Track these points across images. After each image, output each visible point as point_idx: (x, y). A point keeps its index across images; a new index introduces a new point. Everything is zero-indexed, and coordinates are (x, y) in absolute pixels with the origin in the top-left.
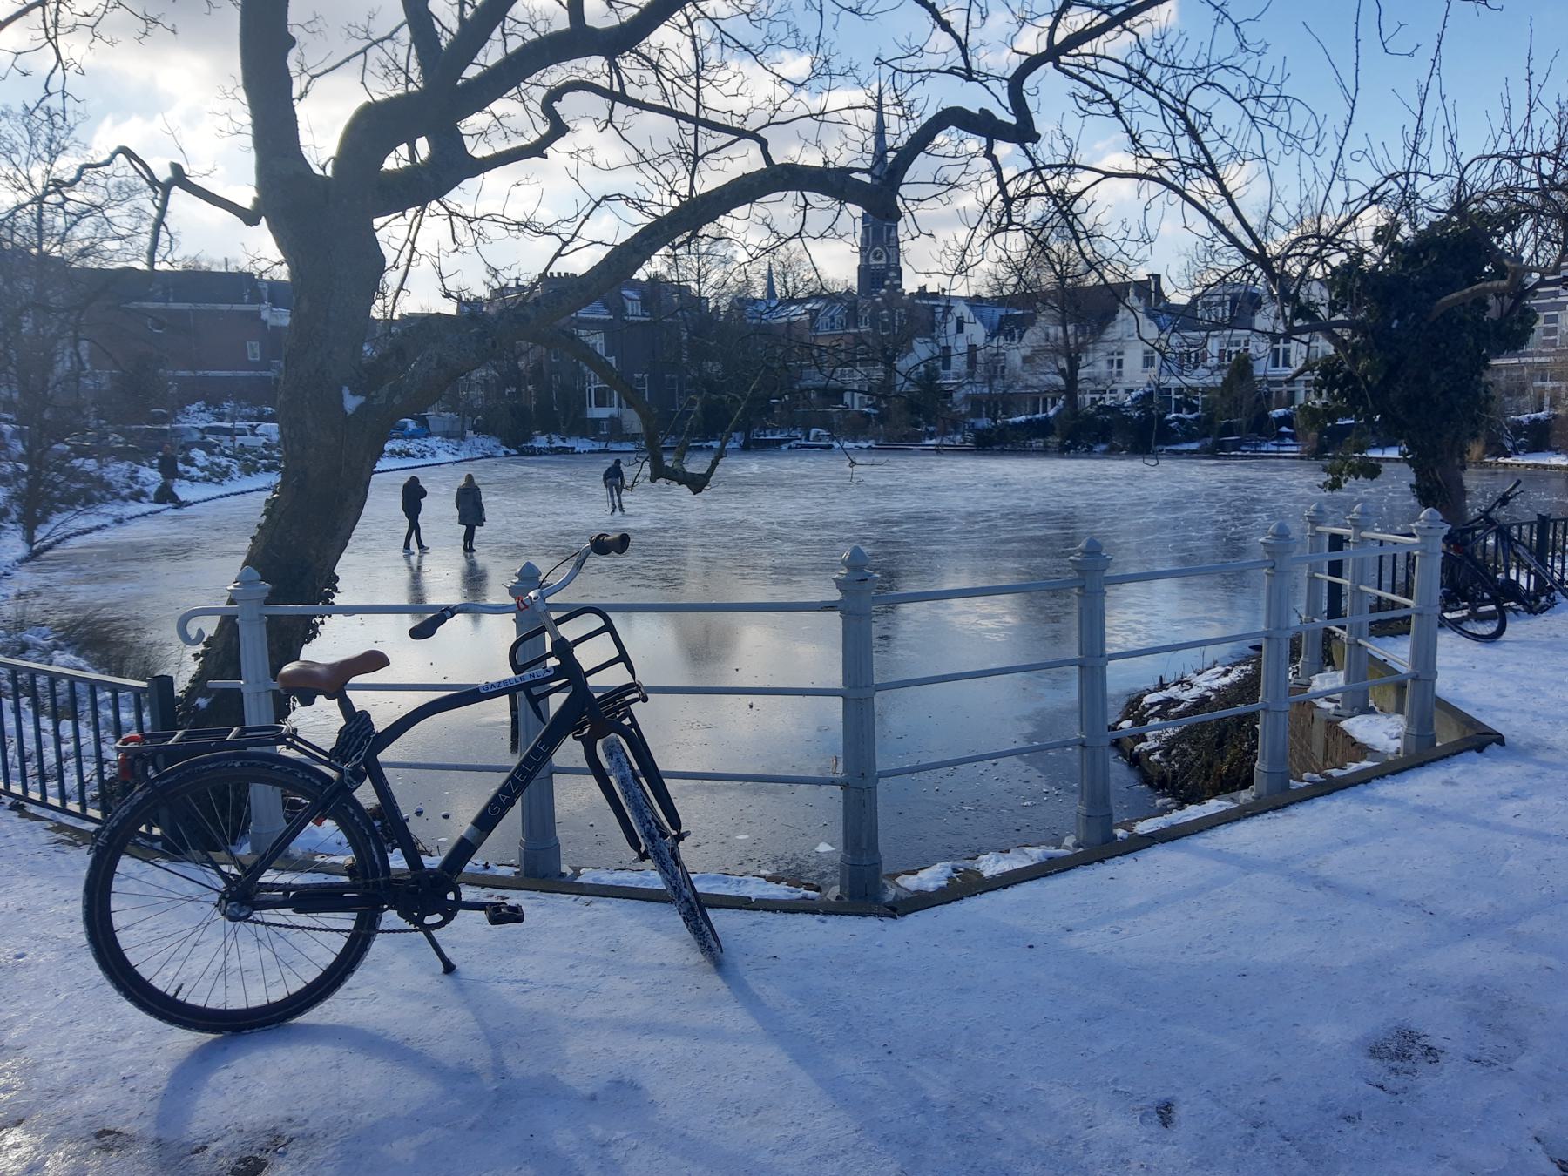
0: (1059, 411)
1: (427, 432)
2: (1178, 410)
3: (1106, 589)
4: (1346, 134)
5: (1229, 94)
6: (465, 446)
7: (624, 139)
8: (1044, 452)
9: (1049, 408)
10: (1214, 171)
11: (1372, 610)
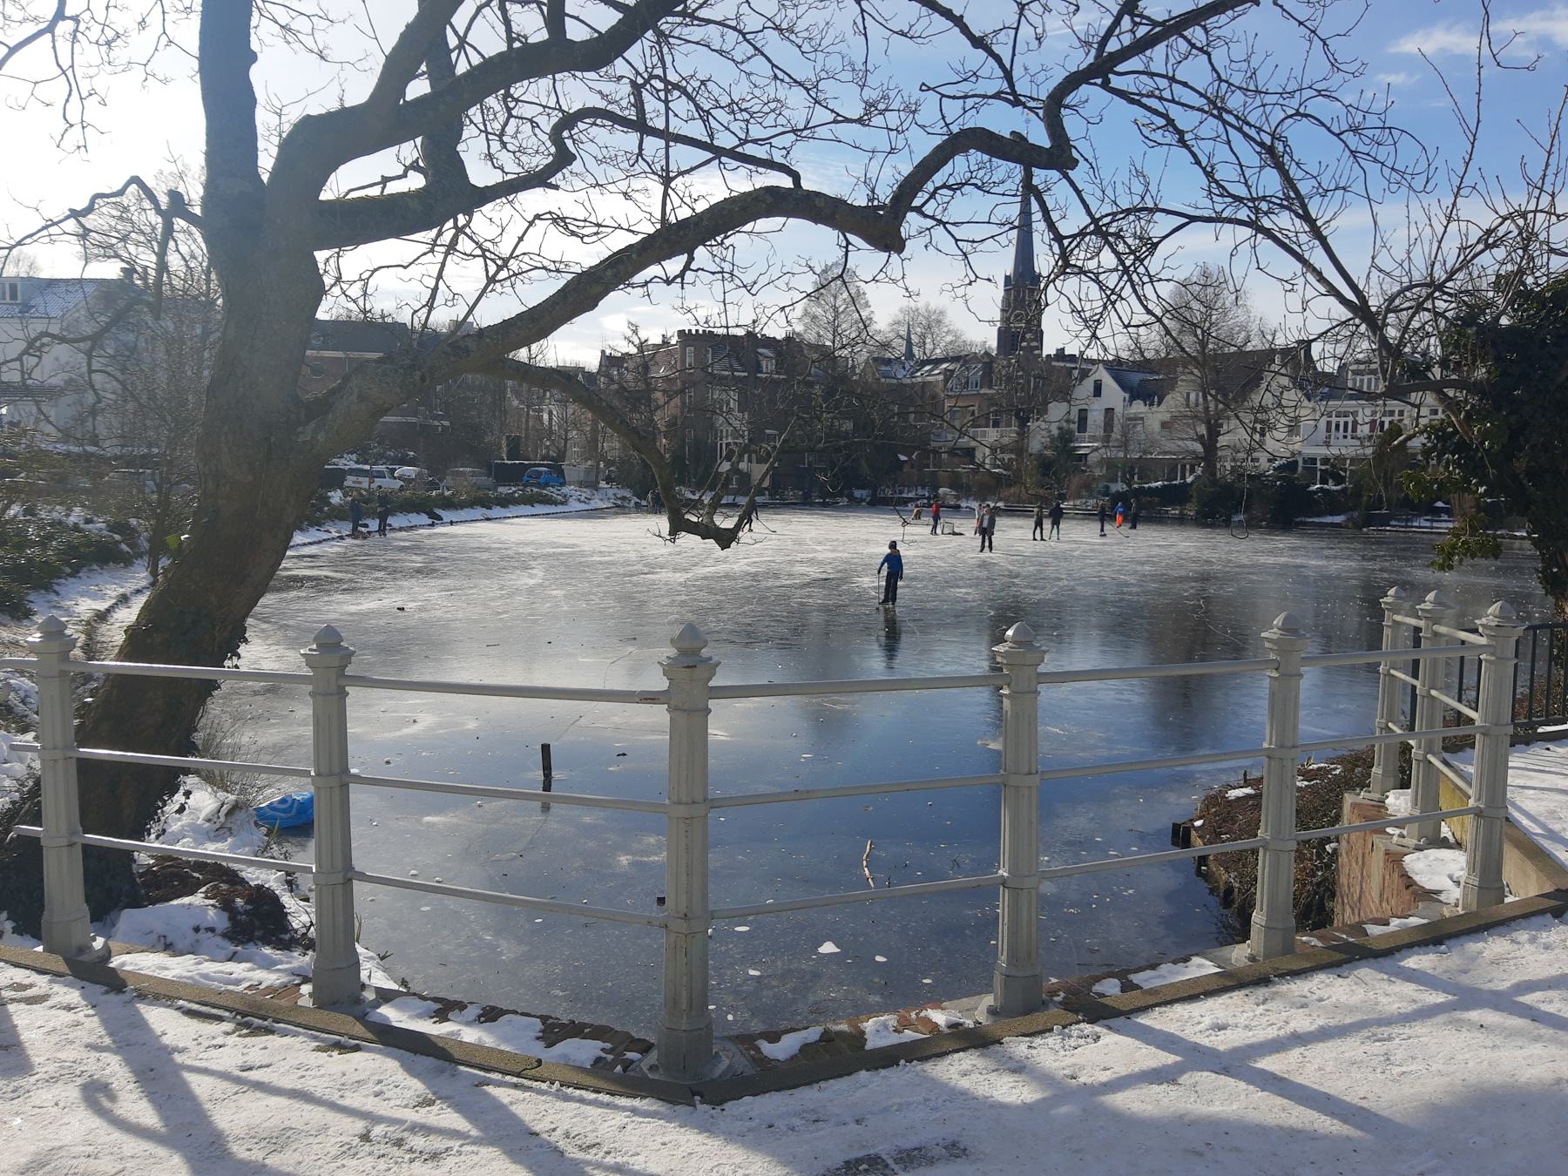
0: (1198, 478)
1: (562, 480)
2: (1324, 481)
3: (1039, 687)
4: (1465, 172)
5: (1323, 124)
6: (597, 496)
7: (54, 47)
8: (1181, 521)
9: (1187, 474)
11: (1446, 724)
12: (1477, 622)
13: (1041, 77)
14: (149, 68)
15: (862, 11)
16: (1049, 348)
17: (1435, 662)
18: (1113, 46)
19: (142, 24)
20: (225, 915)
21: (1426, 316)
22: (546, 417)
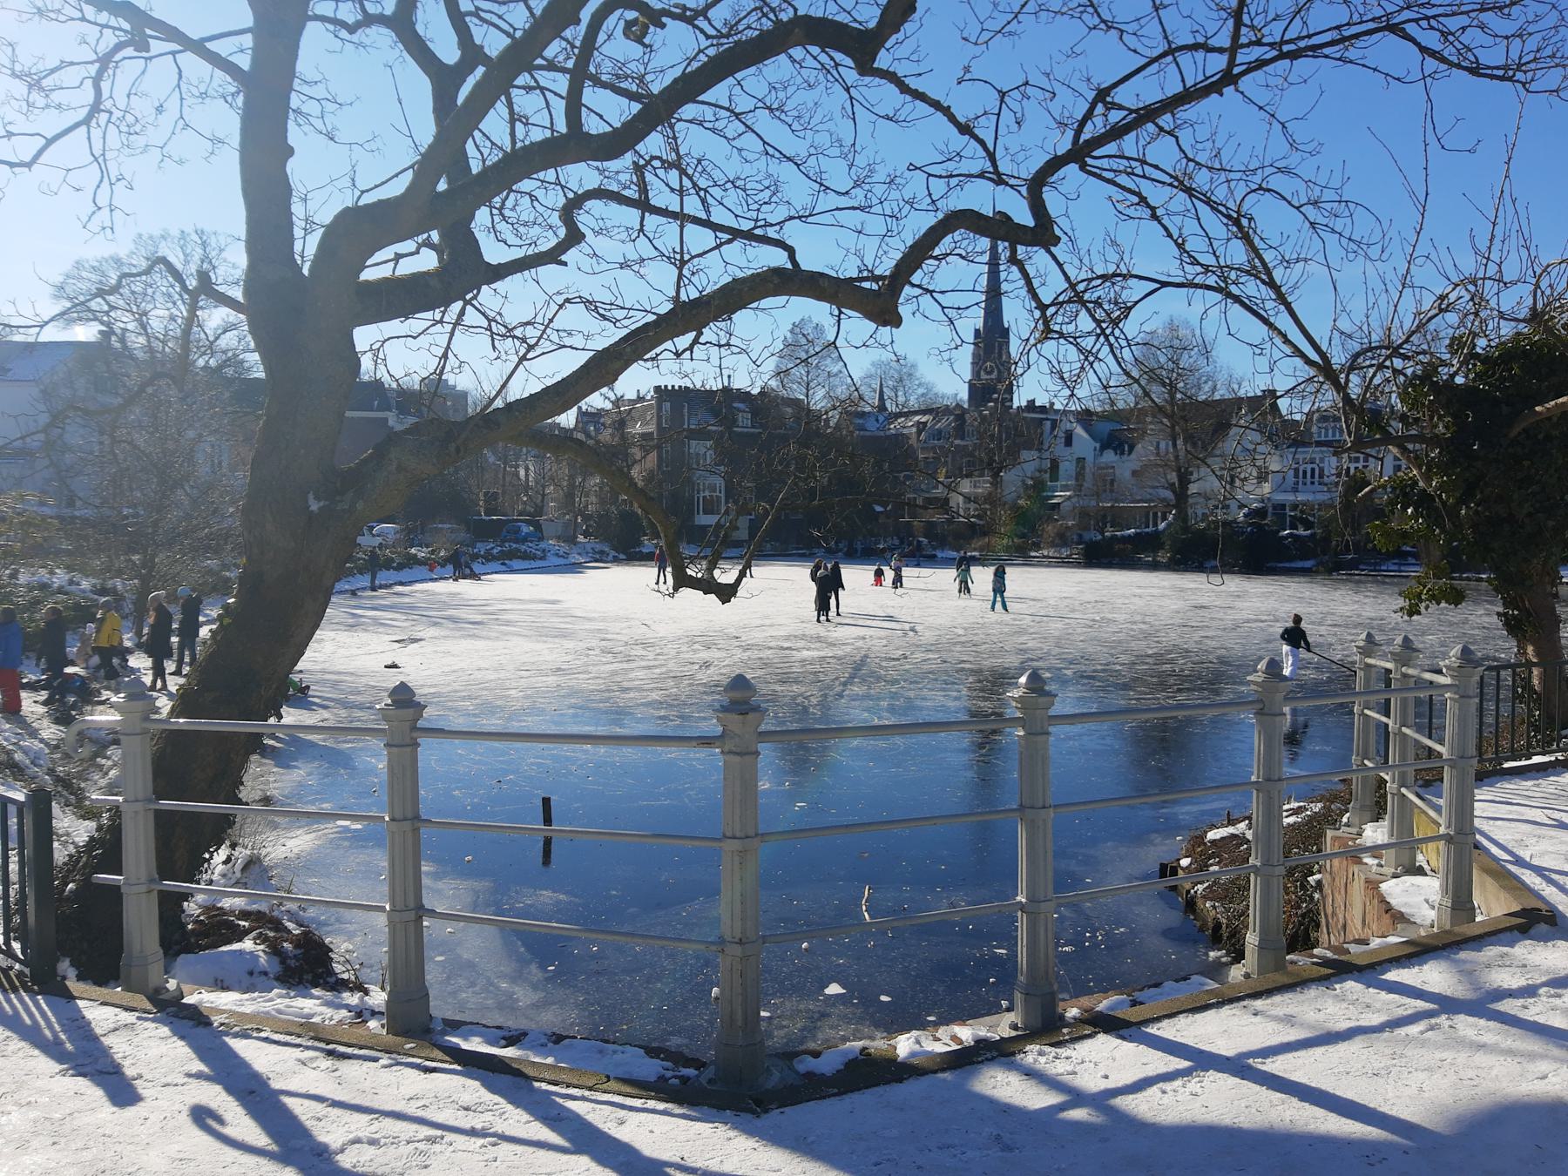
0: (1169, 525)
5: (1285, 199)
7: (89, 138)
8: (1154, 567)
10: (1269, 274)
12: (1441, 663)
13: (1021, 156)
14: (165, 151)
15: (851, 98)
16: (1019, 400)
17: (1404, 701)
18: (1086, 135)
19: (160, 109)
20: (276, 960)
21: (1388, 374)
22: (522, 473)
